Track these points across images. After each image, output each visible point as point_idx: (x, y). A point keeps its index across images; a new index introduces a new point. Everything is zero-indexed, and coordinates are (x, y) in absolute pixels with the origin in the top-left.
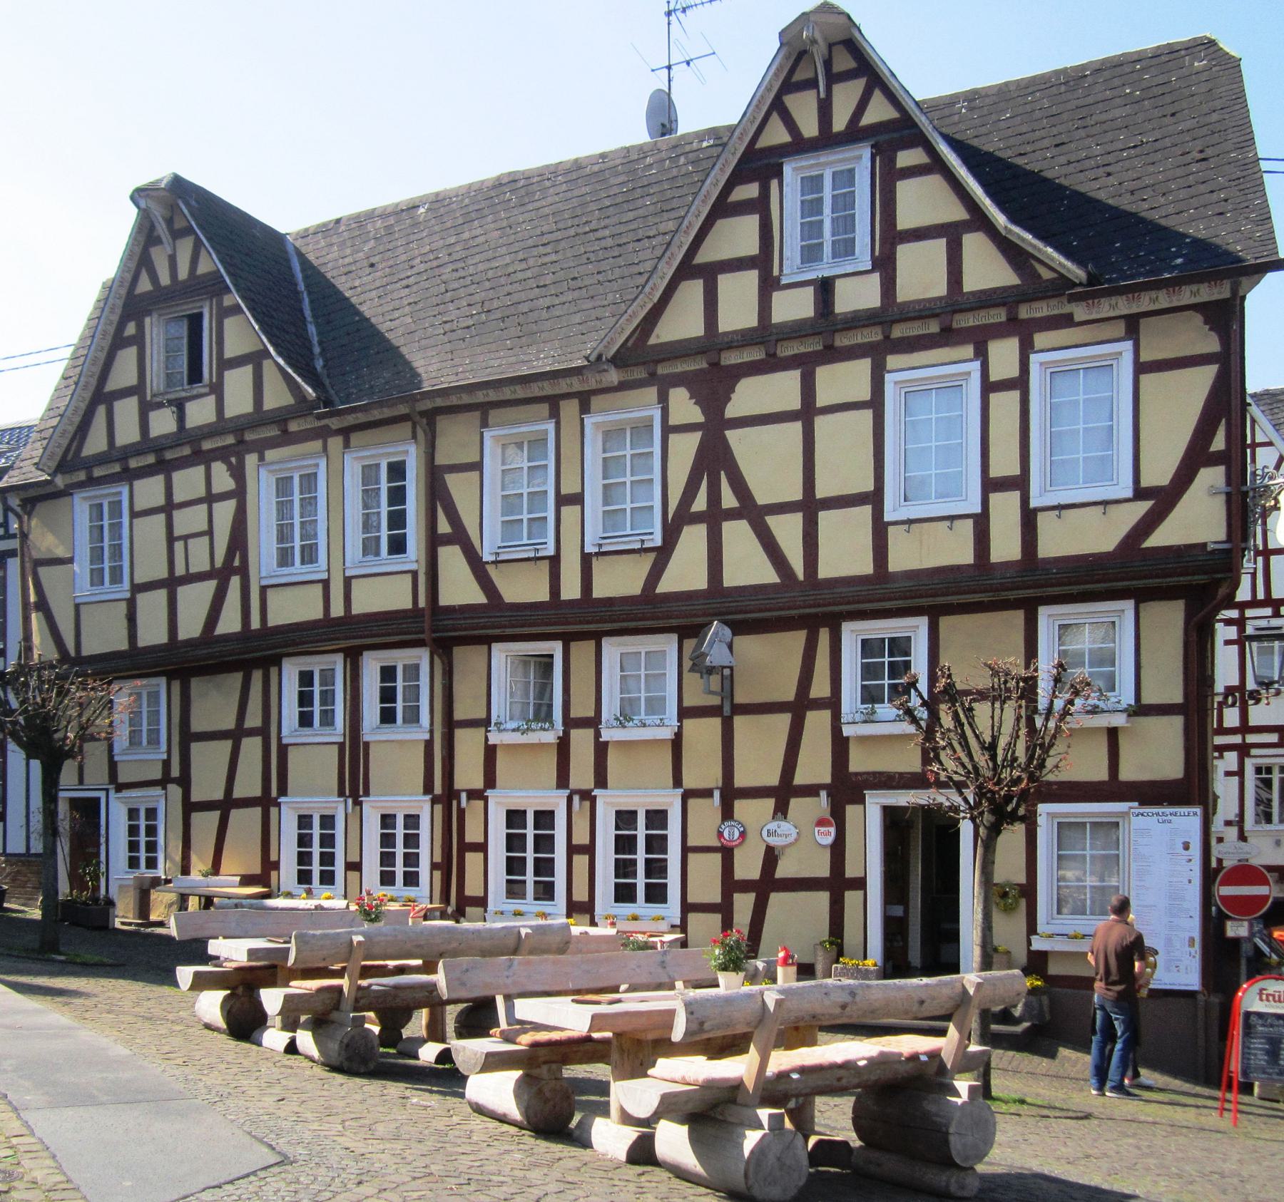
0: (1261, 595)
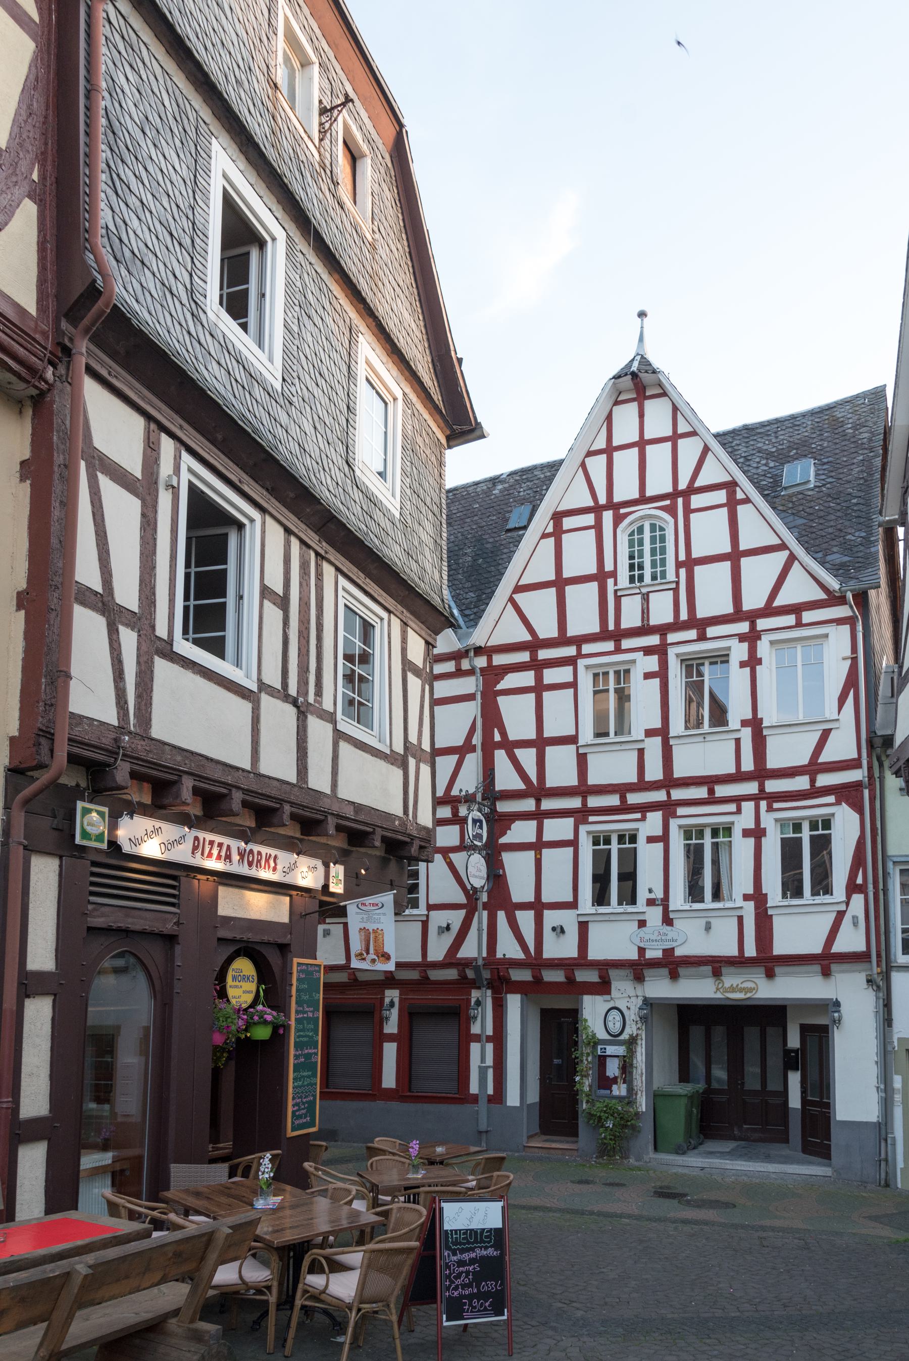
0: (684, 616)
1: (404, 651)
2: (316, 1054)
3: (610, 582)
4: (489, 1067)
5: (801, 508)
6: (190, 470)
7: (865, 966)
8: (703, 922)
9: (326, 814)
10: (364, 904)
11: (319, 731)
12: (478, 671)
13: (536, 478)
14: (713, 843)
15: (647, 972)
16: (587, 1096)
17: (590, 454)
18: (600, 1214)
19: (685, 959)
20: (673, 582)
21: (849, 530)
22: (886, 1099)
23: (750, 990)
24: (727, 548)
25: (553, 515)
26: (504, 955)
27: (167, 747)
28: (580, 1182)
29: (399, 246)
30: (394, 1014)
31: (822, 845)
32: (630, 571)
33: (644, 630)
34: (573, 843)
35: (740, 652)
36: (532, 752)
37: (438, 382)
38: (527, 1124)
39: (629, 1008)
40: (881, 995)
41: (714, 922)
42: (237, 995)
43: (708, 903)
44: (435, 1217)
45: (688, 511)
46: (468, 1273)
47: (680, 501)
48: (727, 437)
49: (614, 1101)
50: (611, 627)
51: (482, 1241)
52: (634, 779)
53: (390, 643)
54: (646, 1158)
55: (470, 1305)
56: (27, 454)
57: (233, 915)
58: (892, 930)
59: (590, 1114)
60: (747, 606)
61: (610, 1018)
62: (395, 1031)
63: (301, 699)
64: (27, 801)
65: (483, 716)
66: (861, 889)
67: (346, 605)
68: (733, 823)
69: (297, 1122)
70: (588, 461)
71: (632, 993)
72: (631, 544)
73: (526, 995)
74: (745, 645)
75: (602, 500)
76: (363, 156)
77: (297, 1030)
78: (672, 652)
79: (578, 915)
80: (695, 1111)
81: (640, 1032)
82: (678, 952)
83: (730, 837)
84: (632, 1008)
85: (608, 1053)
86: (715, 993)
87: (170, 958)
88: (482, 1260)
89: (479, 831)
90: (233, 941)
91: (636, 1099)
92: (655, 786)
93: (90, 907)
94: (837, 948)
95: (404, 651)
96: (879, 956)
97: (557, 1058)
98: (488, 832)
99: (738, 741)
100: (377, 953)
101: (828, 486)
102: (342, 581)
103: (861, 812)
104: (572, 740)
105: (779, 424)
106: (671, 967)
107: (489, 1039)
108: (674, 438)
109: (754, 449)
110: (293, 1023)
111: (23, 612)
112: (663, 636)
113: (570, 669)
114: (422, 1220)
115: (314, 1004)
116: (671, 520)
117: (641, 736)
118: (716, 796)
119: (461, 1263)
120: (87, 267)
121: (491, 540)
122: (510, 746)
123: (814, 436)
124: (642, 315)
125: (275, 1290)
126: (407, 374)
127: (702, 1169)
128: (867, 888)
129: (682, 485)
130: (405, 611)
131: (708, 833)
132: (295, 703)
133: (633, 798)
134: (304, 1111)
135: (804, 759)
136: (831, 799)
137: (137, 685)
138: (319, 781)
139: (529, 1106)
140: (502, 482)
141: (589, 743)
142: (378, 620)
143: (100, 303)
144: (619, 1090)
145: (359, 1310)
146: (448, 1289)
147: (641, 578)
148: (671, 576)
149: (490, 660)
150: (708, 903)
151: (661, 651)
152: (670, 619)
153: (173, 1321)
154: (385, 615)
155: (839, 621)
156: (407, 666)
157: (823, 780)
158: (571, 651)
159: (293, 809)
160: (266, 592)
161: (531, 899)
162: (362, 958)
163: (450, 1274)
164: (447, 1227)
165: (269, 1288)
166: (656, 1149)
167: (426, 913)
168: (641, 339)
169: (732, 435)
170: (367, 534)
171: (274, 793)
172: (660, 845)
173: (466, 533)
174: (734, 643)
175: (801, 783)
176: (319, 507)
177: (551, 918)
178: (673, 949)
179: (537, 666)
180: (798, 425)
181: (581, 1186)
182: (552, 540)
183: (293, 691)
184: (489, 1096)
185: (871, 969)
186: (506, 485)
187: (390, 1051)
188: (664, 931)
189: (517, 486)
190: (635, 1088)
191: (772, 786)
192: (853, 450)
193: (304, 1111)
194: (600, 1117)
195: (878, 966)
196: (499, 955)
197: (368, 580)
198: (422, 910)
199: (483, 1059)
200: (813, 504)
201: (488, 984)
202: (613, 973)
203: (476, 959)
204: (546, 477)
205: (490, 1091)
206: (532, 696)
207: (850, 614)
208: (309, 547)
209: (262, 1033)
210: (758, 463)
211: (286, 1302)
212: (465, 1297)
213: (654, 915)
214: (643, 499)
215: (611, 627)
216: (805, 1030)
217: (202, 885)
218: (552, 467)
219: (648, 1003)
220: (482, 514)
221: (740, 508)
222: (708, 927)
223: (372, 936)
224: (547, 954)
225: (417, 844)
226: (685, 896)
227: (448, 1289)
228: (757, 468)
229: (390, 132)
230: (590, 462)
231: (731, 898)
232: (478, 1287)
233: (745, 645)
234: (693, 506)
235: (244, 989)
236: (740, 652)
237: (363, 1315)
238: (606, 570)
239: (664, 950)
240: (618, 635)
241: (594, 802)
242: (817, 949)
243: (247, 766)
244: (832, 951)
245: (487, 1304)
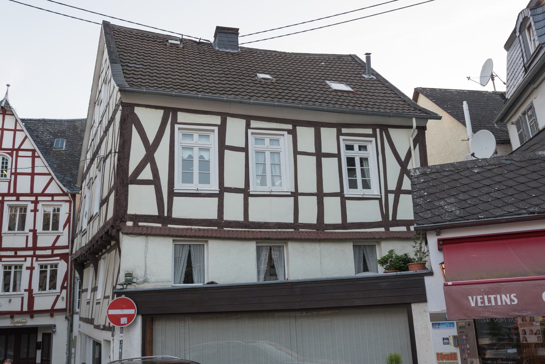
5: (59, 157)
7: (65, 313)
8: (8, 299)
21: (74, 169)
22: (69, 356)
23: (24, 322)
31: (54, 274)
35: (31, 206)
40: (70, 322)
45: (17, 156)
47: (15, 152)
58: (75, 301)
60: (35, 191)
66: (66, 288)
68: (23, 264)
74: (33, 205)
78: (6, 204)
83: (21, 269)
86: (11, 324)
94: (56, 307)
96: (70, 310)
99: (27, 237)
101: (69, 151)
103: (68, 263)
105: (55, 122)
108: (15, 130)
116: (10, 158)
123: (67, 130)
124: (8, 85)
128: (67, 287)
129: (16, 147)
131: (13, 268)
135: (50, 244)
136: (58, 258)
148: (8, 177)
150: (11, 292)
155: (66, 201)
157: (56, 252)
168: (7, 94)
174: (29, 203)
175: (49, 252)
180: (62, 124)
185: (67, 314)
191: (38, 253)
192: (79, 140)
195: (69, 313)
200: (63, 156)
207: (69, 199)
210: (46, 135)
216: (44, 335)
221: (36, 159)
222: (10, 301)
226: (2, 290)
228: (46, 137)
231: (20, 291)
233: (33, 205)
234: (19, 155)
236: (31, 206)
242: (49, 308)
244: (54, 308)
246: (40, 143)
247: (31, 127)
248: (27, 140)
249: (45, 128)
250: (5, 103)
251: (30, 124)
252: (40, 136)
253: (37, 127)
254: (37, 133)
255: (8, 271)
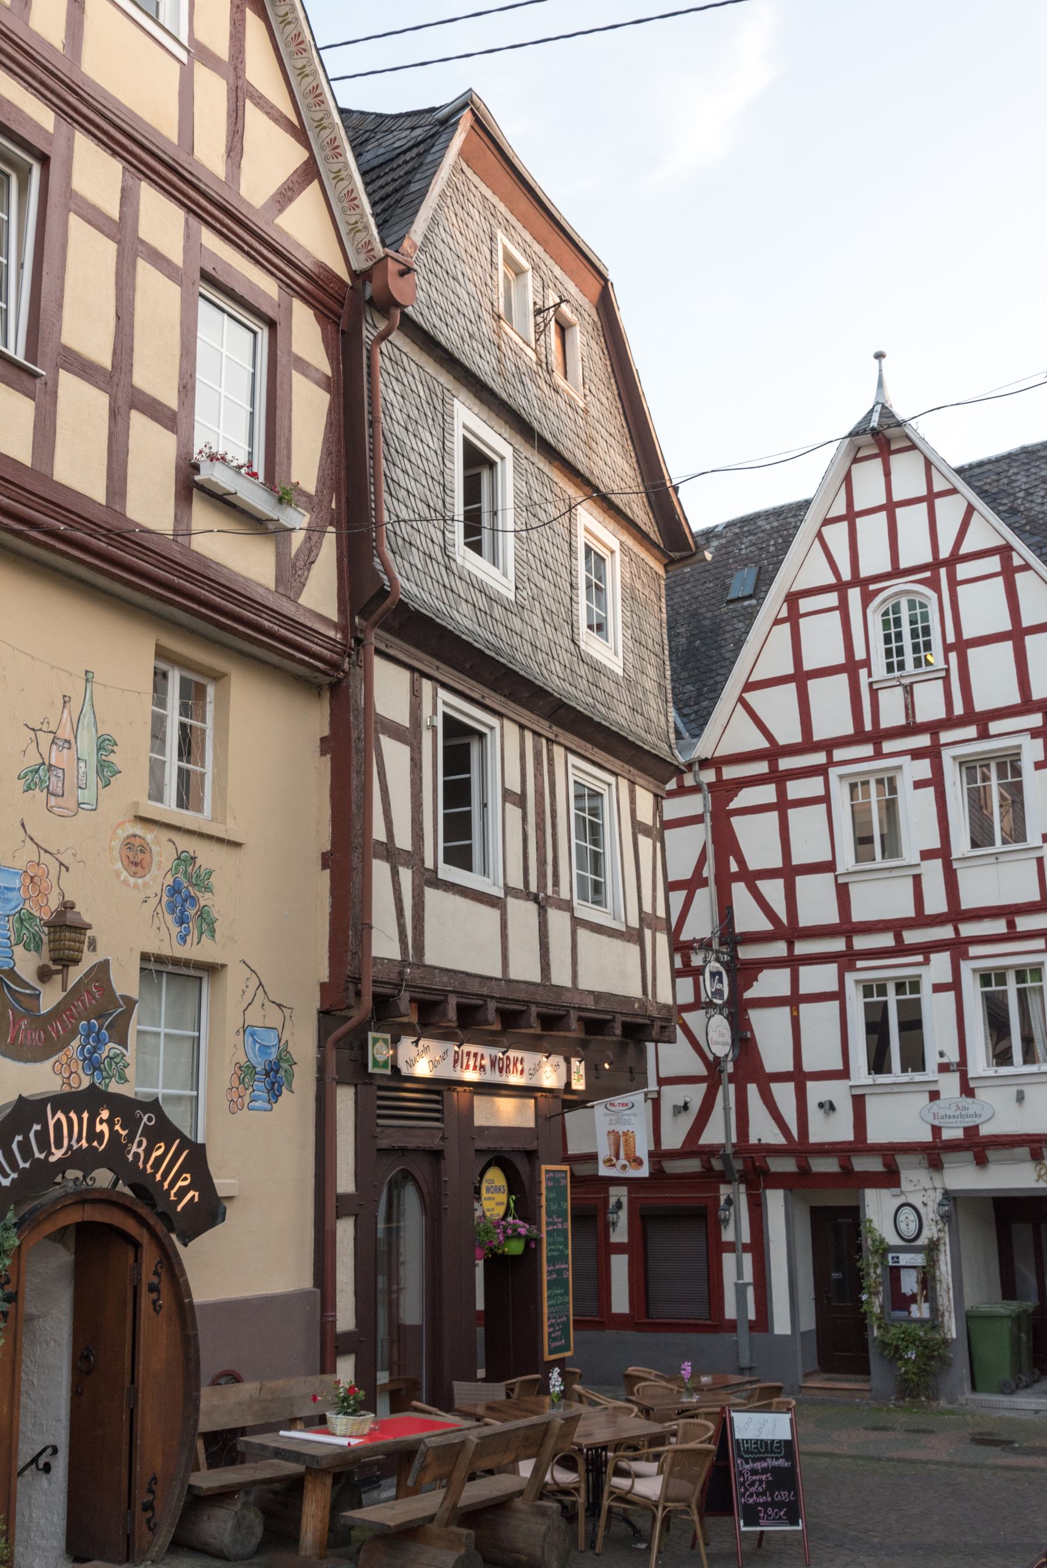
0: (959, 709)
1: (633, 811)
2: (567, 1270)
3: (863, 673)
4: (748, 1284)
6: (445, 703)
8: (1013, 1091)
9: (567, 1009)
10: (613, 1105)
11: (558, 921)
12: (705, 787)
13: (759, 530)
14: (1019, 990)
15: (946, 1157)
16: (879, 1319)
17: (827, 522)
18: (899, 1460)
19: (993, 1139)
20: (942, 669)
24: (1005, 625)
25: (787, 596)
26: (759, 1140)
27: (437, 971)
28: (876, 1429)
29: (609, 394)
30: (623, 1216)
32: (887, 658)
33: (910, 729)
34: (839, 995)
36: (779, 883)
37: (653, 512)
38: (802, 1358)
39: (925, 1205)
41: (1028, 1091)
42: (491, 1207)
43: (1019, 1067)
44: (724, 1428)
46: (761, 1482)
47: (943, 571)
48: (1001, 464)
49: (913, 1325)
50: (868, 727)
51: (772, 1452)
52: (911, 913)
53: (619, 808)
54: (962, 1399)
55: (766, 1512)
56: (326, 732)
57: (486, 1124)
59: (882, 1342)
61: (901, 1217)
62: (625, 1239)
63: (542, 895)
64: (338, 1040)
65: (715, 841)
67: (576, 782)
69: (553, 1345)
70: (827, 531)
71: (928, 1184)
72: (886, 624)
73: (790, 1190)
75: (846, 575)
76: (572, 325)
77: (549, 1244)
78: (947, 755)
79: (851, 1087)
80: (1023, 1336)
81: (942, 1235)
82: (985, 1131)
83: (1041, 980)
84: (930, 1204)
85: (902, 1263)
86: (1037, 1181)
87: (437, 1173)
88: (774, 1470)
89: (719, 986)
90: (487, 1151)
91: (943, 1322)
92: (938, 920)
93: (378, 1130)
95: (633, 811)
97: (836, 1271)
98: (730, 985)
100: (627, 1158)
102: (573, 759)
104: (828, 867)
106: (976, 1149)
107: (746, 1248)
108: (930, 498)
109: (1036, 479)
110: (544, 1235)
111: (328, 871)
112: (935, 736)
113: (820, 779)
114: (710, 1434)
115: (562, 1214)
117: (916, 859)
118: (1018, 929)
119: (754, 1472)
120: (375, 572)
121: (709, 615)
122: (751, 878)
124: (879, 356)
125: (583, 1492)
126: (623, 522)
127: (1037, 1412)
129: (945, 553)
130: (632, 769)
131: (1011, 977)
132: (535, 899)
133: (911, 937)
134: (558, 1333)
137: (413, 917)
138: (561, 977)
139: (803, 1334)
140: (718, 536)
141: (851, 869)
142: (606, 787)
143: (388, 602)
144: (920, 1311)
145: (665, 1508)
146: (743, 1495)
147: (901, 666)
149: (719, 773)
150: (1019, 1067)
151: (933, 753)
152: (941, 714)
153: (519, 1500)
154: (612, 779)
156: (638, 827)
158: (820, 758)
159: (539, 1009)
160: (507, 795)
161: (790, 1067)
162: (609, 1163)
163: (744, 1482)
164: (738, 1436)
165: (577, 1489)
166: (974, 1388)
167: (657, 1088)
168: (880, 384)
169: (1007, 461)
170: (594, 707)
171: (523, 996)
172: (951, 995)
173: (677, 606)
174: (1025, 740)
176: (551, 699)
177: (816, 1091)
178: (977, 1127)
179: (779, 778)
181: (877, 1433)
182: (787, 627)
183: (533, 888)
184: (750, 1321)
186: (723, 541)
187: (620, 1266)
188: (964, 1104)
189: (737, 542)
190: (941, 1308)
193: (558, 1333)
194: (897, 1348)
196: (753, 1140)
197: (595, 749)
198: (653, 1086)
199: (740, 1274)
201: (741, 1177)
202: (901, 1160)
203: (723, 1146)
204: (772, 528)
205: (752, 1316)
206: (775, 815)
208: (540, 735)
209: (516, 1248)
211: (593, 1508)
212: (761, 1505)
213: (950, 1084)
214: (897, 572)
215: (868, 727)
217: (460, 1096)
218: (780, 515)
219: (950, 1197)
220: (696, 580)
221: (1018, 577)
222: (1020, 1098)
223: (622, 1140)
224: (814, 1138)
225: (658, 1024)
227: (743, 1495)
229: (596, 288)
230: (828, 531)
232: (772, 1496)
234: (960, 577)
235: (496, 1200)
237: (669, 1512)
238: (857, 658)
239: (966, 1129)
240: (878, 737)
241: (861, 943)
243: (499, 975)
245: (782, 1513)
246: (1028, 528)
247: (987, 487)
248: (975, 519)
249: (1033, 477)
250: (881, 416)
251: (981, 477)
252: (1022, 508)
253: (1006, 481)
254: (1012, 499)
255: (994, 992)
